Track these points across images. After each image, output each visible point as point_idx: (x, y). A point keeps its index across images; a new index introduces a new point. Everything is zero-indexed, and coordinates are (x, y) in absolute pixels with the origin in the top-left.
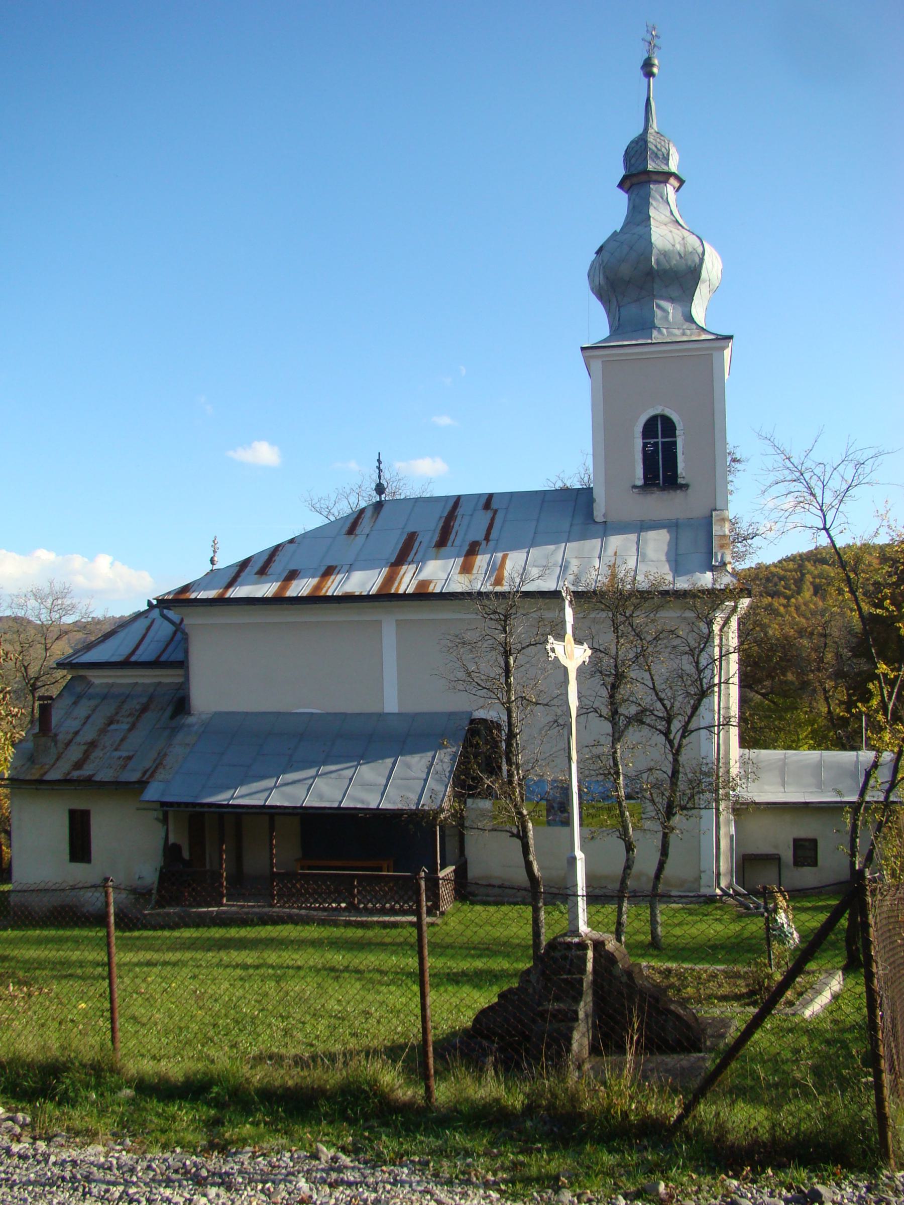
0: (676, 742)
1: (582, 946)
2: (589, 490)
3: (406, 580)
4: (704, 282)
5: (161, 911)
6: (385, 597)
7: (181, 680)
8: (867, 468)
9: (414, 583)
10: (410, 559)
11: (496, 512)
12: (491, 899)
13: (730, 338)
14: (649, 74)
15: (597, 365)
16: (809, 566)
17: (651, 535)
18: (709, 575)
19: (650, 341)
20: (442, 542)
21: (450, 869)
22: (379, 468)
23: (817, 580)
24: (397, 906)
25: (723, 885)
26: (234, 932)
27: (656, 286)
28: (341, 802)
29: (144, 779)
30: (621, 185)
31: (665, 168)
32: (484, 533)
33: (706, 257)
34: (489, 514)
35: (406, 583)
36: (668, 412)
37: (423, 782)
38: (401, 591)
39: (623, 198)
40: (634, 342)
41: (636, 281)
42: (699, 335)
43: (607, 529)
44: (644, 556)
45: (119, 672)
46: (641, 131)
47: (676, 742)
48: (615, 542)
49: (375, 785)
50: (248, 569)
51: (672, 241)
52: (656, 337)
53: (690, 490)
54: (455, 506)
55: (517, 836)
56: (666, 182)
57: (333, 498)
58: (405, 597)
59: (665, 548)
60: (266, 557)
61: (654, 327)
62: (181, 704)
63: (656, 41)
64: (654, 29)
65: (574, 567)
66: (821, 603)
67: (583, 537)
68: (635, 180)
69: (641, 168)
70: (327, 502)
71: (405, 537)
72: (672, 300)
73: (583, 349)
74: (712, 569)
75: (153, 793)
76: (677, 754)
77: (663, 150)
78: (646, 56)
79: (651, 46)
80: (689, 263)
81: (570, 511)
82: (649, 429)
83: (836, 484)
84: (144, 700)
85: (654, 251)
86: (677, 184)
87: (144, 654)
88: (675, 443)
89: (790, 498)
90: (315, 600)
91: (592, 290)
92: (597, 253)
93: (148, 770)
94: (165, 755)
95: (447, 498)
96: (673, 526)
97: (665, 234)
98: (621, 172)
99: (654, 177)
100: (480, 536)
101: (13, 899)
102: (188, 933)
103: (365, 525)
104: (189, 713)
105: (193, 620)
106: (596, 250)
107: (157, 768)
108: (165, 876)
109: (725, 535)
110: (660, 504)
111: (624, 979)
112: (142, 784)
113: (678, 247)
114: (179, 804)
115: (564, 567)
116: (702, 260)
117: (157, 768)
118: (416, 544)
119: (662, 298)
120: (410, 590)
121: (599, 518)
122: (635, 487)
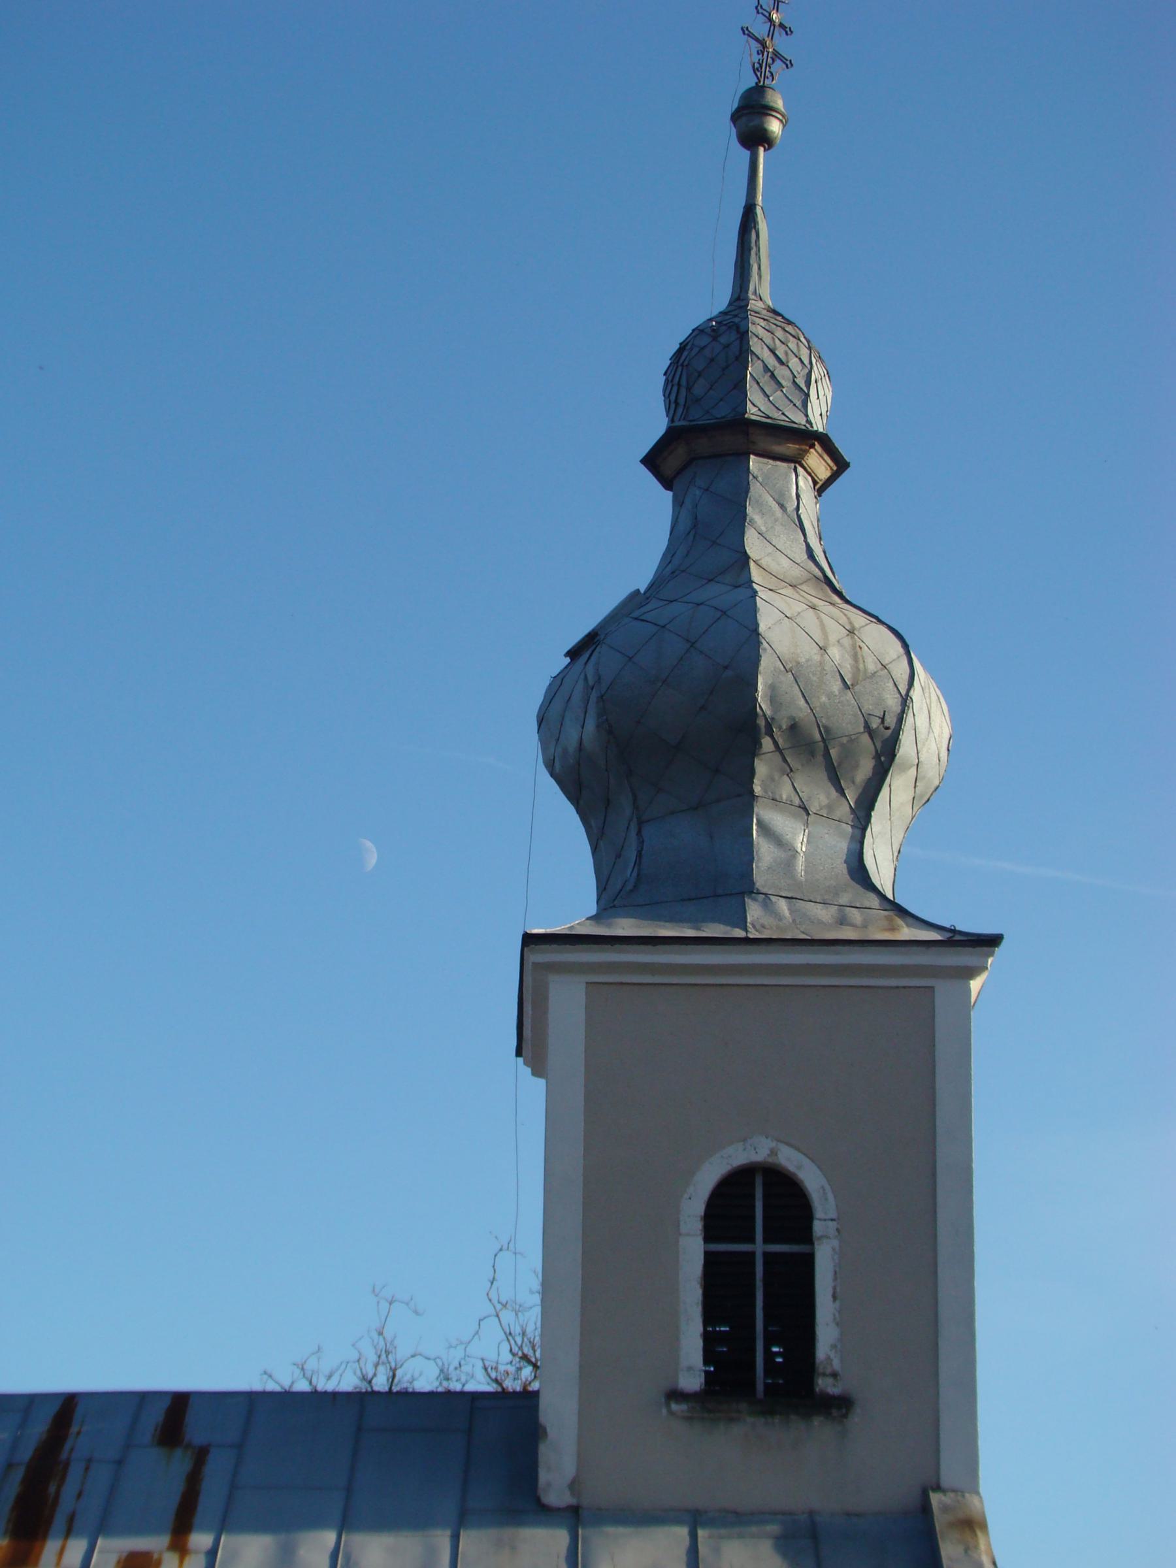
2: (528, 1399)
4: (904, 768)
11: (201, 1455)
13: (991, 941)
14: (754, 138)
15: (568, 1001)
19: (739, 933)
30: (652, 461)
31: (799, 419)
34: (180, 1463)
36: (790, 1159)
41: (667, 740)
46: (721, 301)
53: (856, 1418)
63: (780, 43)
69: (723, 412)
73: (529, 940)
78: (751, 81)
79: (767, 58)
82: (729, 1206)
85: (767, 663)
88: (807, 1263)
91: (550, 766)
92: (574, 654)
98: (656, 425)
121: (556, 1494)
122: (675, 1395)
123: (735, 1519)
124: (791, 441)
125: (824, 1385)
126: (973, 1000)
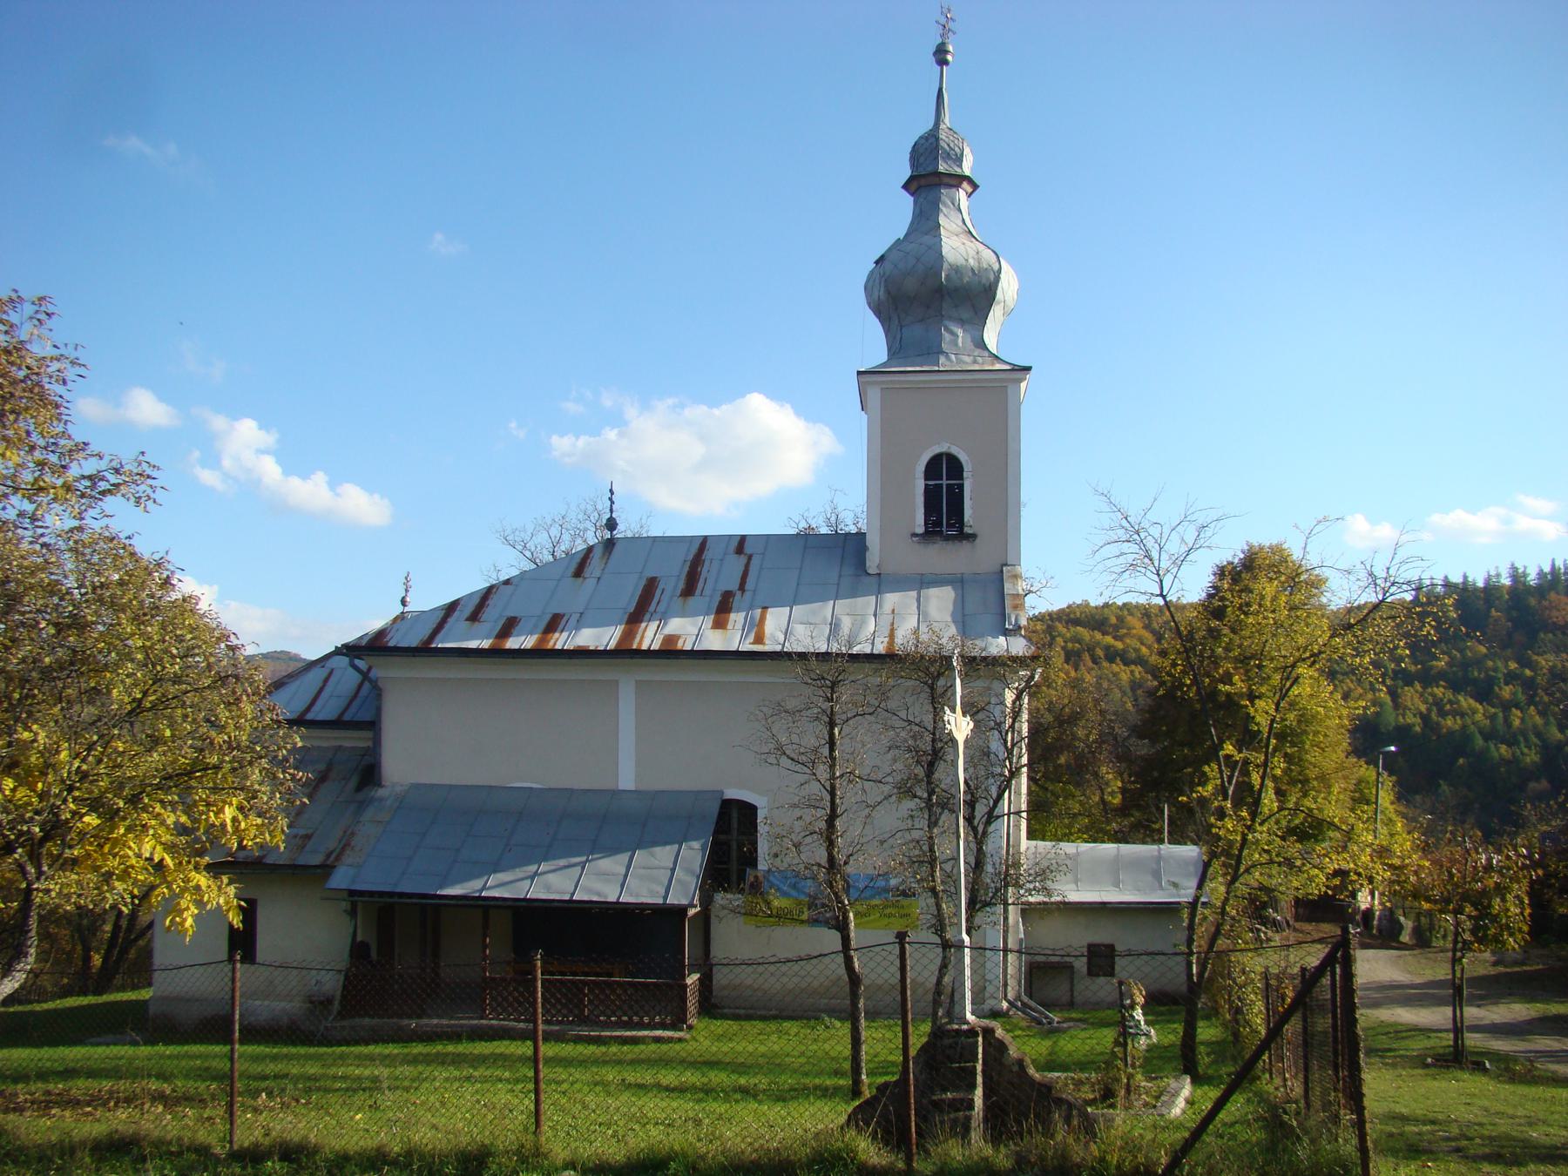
0: (980, 829)
1: (972, 1033)
2: (861, 536)
3: (650, 633)
5: (345, 1023)
6: (624, 653)
7: (370, 744)
8: (1208, 532)
9: (660, 638)
10: (652, 608)
11: (750, 557)
12: (742, 1012)
13: (1028, 369)
14: (942, 62)
15: (874, 395)
16: (1060, 627)
18: (1002, 638)
20: (689, 590)
21: (696, 976)
23: (1070, 645)
25: (1010, 996)
26: (463, 1048)
27: (945, 305)
30: (906, 187)
32: (738, 581)
34: (743, 559)
35: (649, 637)
36: (955, 451)
38: (644, 647)
41: (923, 300)
43: (882, 583)
44: (926, 614)
45: (343, 733)
46: (931, 125)
47: (980, 829)
48: (891, 599)
55: (837, 929)
56: (958, 186)
58: (649, 654)
59: (951, 607)
60: (476, 601)
62: (369, 774)
63: (951, 25)
65: (846, 624)
66: (1073, 674)
67: (854, 594)
68: (923, 182)
69: (930, 169)
72: (962, 322)
74: (1006, 633)
75: (341, 879)
78: (939, 41)
81: (836, 559)
83: (1174, 547)
84: (322, 767)
85: (945, 266)
86: (970, 190)
87: (321, 712)
88: (961, 487)
89: (1122, 560)
92: (877, 262)
94: (353, 834)
96: (958, 582)
97: (957, 246)
98: (906, 173)
99: (946, 180)
100: (733, 585)
101: (152, 1010)
104: (380, 785)
105: (385, 671)
107: (343, 849)
110: (943, 557)
111: (1016, 1068)
112: (326, 869)
113: (971, 262)
114: (371, 894)
115: (835, 627)
116: (997, 279)
117: (343, 849)
118: (658, 592)
119: (950, 318)
121: (872, 567)
122: (914, 535)
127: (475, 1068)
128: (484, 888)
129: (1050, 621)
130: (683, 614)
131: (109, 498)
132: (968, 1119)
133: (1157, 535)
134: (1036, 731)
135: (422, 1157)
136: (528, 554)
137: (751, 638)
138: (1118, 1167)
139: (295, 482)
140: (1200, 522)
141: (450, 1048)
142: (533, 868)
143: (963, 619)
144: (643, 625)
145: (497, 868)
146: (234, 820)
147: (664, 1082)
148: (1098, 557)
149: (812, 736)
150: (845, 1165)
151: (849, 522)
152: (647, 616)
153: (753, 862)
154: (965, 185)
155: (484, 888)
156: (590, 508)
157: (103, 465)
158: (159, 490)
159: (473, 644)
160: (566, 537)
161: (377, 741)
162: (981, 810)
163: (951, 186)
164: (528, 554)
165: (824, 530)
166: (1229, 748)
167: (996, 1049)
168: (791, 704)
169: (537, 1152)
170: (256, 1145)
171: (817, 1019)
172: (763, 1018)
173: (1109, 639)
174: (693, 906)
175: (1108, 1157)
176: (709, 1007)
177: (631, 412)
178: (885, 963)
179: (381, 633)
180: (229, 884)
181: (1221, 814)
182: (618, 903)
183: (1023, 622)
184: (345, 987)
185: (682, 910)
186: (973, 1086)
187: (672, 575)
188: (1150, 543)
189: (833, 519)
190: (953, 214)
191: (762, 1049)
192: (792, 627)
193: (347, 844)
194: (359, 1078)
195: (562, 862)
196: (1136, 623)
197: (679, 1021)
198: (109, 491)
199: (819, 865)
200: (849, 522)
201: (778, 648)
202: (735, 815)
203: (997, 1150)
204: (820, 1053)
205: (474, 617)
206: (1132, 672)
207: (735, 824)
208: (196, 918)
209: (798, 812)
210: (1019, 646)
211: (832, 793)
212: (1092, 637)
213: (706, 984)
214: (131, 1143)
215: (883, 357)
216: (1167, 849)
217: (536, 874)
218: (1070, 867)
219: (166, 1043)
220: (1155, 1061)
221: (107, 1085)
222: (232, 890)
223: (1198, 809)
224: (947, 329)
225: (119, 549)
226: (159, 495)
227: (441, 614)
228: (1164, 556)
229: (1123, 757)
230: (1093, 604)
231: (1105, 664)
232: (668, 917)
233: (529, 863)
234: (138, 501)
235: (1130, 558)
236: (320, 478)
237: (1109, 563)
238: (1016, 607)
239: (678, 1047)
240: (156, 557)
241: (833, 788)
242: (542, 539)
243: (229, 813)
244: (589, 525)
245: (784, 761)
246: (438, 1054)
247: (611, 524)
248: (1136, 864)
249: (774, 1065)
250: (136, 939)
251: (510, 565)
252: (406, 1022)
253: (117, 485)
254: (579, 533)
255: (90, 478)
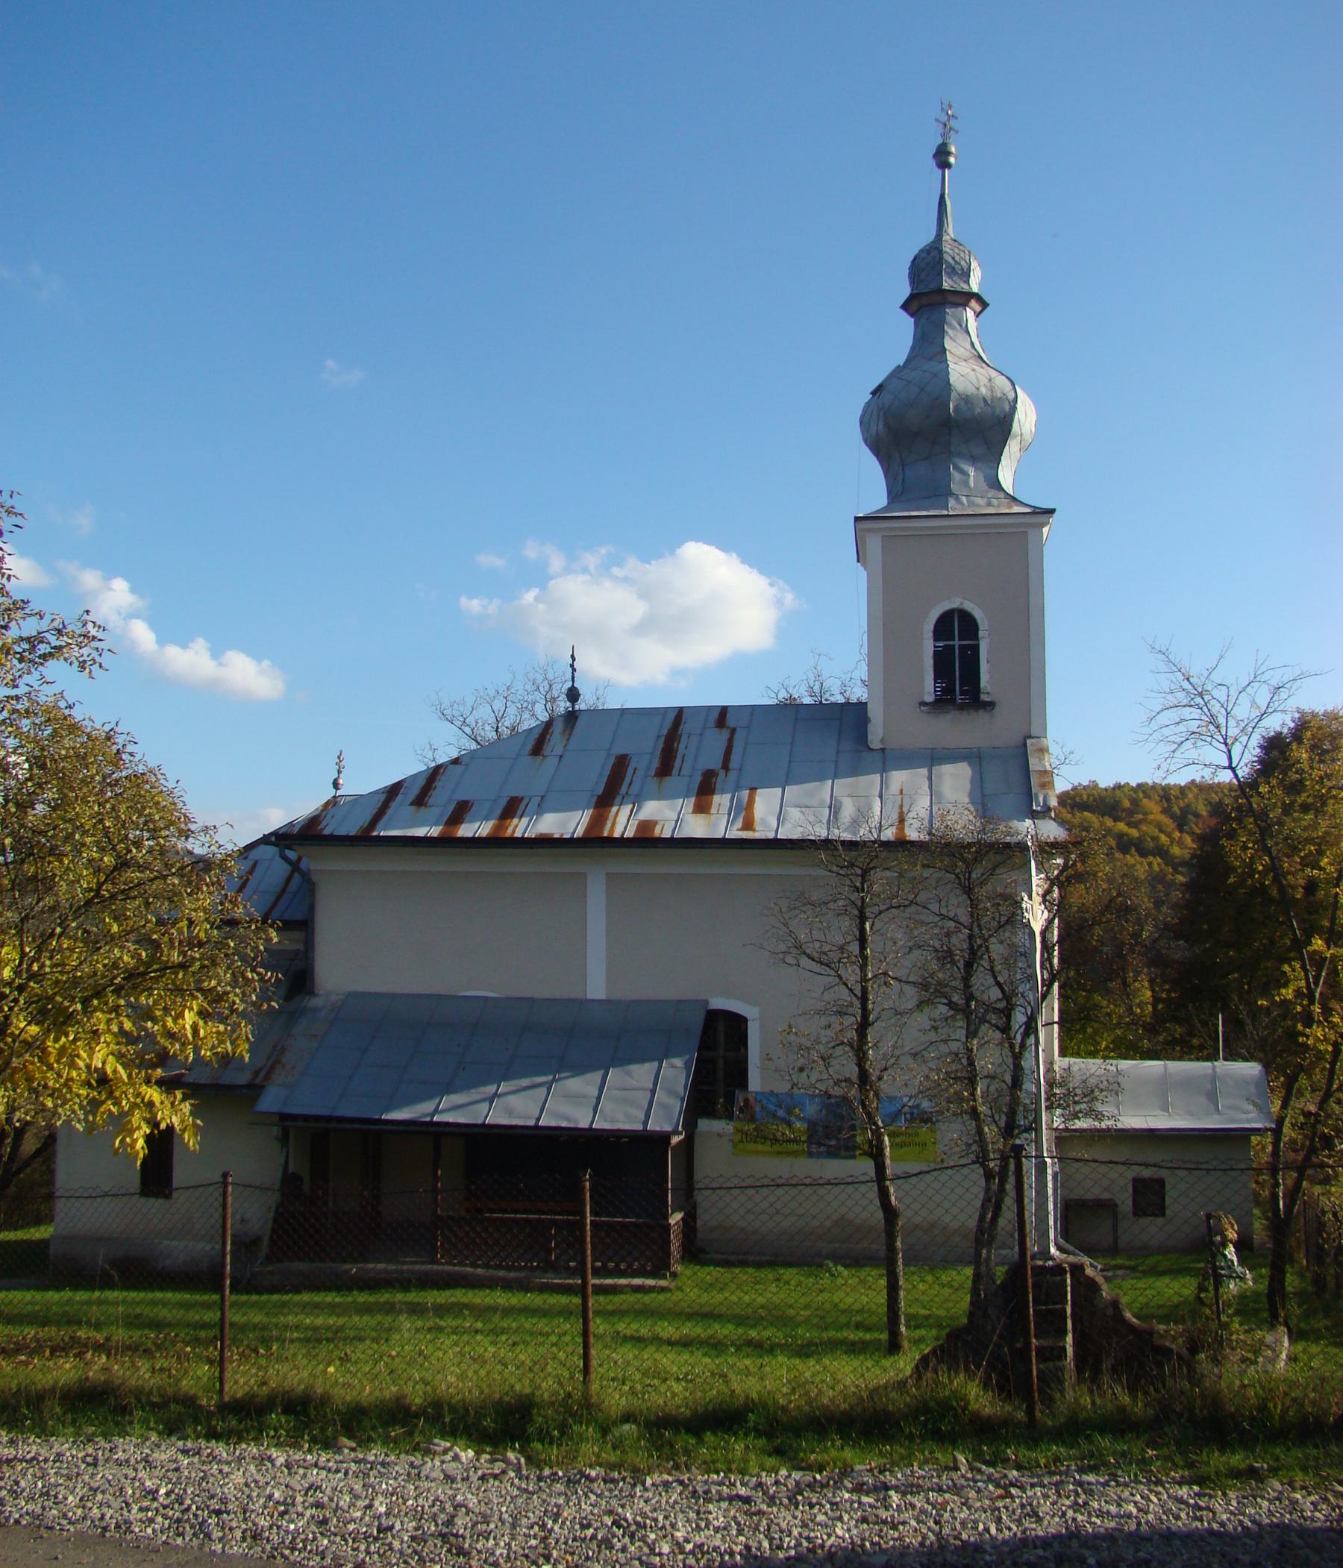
1: (1059, 1269)
2: (861, 706)
4: (1015, 437)
6: (594, 842)
7: (301, 947)
8: (1283, 694)
10: (623, 789)
11: (733, 731)
14: (943, 165)
15: (874, 545)
17: (947, 769)
18: (1028, 822)
19: (945, 512)
20: (665, 767)
22: (572, 666)
24: (623, 1266)
28: (538, 1119)
29: (258, 1081)
30: (905, 307)
31: (965, 287)
33: (1019, 405)
34: (725, 734)
35: (622, 822)
36: (969, 606)
37: (649, 1094)
38: (617, 834)
39: (909, 322)
40: (925, 513)
41: (927, 434)
42: (1010, 507)
43: (887, 760)
44: (940, 795)
46: (932, 237)
48: (899, 778)
49: (584, 1097)
50: (399, 798)
51: (975, 382)
52: (953, 507)
53: (997, 709)
54: (675, 724)
55: (871, 1155)
56: (965, 305)
57: (470, 702)
58: (622, 842)
59: (968, 786)
60: (422, 782)
61: (950, 494)
63: (952, 123)
64: (950, 107)
65: (848, 810)
67: (855, 772)
68: (925, 300)
69: (933, 286)
70: (461, 708)
71: (612, 761)
72: (974, 460)
73: (857, 519)
74: (1034, 815)
75: (270, 1101)
76: (1017, 1057)
77: (963, 263)
78: (940, 141)
79: (946, 129)
80: (998, 412)
81: (830, 734)
82: (944, 626)
85: (953, 395)
86: (978, 308)
88: (976, 649)
89: (1181, 727)
90: (496, 842)
91: (865, 441)
92: (874, 393)
93: (261, 1069)
94: (283, 1049)
95: (666, 710)
96: (975, 757)
97: (966, 374)
98: (906, 291)
99: (951, 298)
100: (715, 763)
101: (52, 1250)
102: (330, 1297)
103: (556, 743)
104: (312, 992)
105: (316, 862)
106: (872, 389)
108: (281, 1219)
109: (1045, 771)
110: (957, 729)
112: (254, 1090)
113: (983, 390)
114: (306, 1118)
115: (835, 809)
116: (1013, 409)
118: (630, 772)
119: (960, 455)
120: (630, 833)
121: (875, 742)
122: (923, 704)
123: (951, 756)
124: (965, 298)
125: (984, 697)
126: (1056, 921)
127: (441, 1318)
128: (436, 1111)
129: (1077, 801)
130: (659, 797)
131: (51, 663)
132: (1062, 1369)
133: (1223, 699)
134: (1074, 931)
135: (453, 1409)
136: (468, 730)
137: (739, 824)
138: (1282, 1417)
139: (173, 651)
140: (1274, 683)
141: (399, 1296)
142: (491, 1089)
143: (982, 801)
144: (614, 809)
145: (449, 1089)
146: (195, 1029)
147: (665, 1335)
148: (1154, 725)
149: (840, 931)
150: (955, 1415)
151: (836, 690)
152: (618, 799)
153: (743, 1083)
154: (973, 303)
155: (436, 1111)
156: (540, 678)
157: (44, 625)
158: (106, 653)
159: (420, 832)
160: (512, 710)
161: (309, 944)
162: (1019, 1018)
163: (957, 305)
164: (468, 730)
165: (807, 700)
166: (1318, 943)
167: (1086, 1288)
168: (816, 896)
169: (587, 1404)
170: (251, 1396)
171: (821, 1265)
172: (759, 1265)
173: (1121, 826)
174: (676, 1132)
175: (1271, 1405)
176: (694, 1253)
177: (557, 563)
178: (865, 1202)
179: (314, 821)
180: (183, 1100)
181: (1308, 1020)
182: (590, 1129)
183: (1053, 802)
184: (274, 1230)
185: (664, 1138)
186: (1065, 1333)
187: (645, 753)
188: (1215, 707)
189: (817, 688)
190: (961, 337)
191: (761, 1300)
192: (781, 812)
193: (278, 1061)
194: (316, 1329)
195: (525, 1082)
196: (1153, 807)
197: (660, 1268)
198: (51, 654)
199: (847, 1080)
200: (836, 690)
201: (771, 835)
202: (721, 1027)
203: (1134, 1398)
204: (827, 1306)
205: (420, 801)
206: (1150, 864)
207: (721, 1038)
208: (149, 1139)
209: (824, 1021)
210: (1051, 830)
211: (864, 999)
212: (1102, 824)
213: (689, 1222)
214: (103, 1392)
215: (883, 501)
216: (1223, 1066)
217: (495, 1095)
218: (1114, 1087)
219: (75, 1288)
220: (1245, 1307)
221: (30, 1332)
222: (186, 1107)
223: (1248, 1021)
224: (956, 468)
225: (60, 722)
226: (106, 659)
227: (383, 797)
228: (1232, 723)
229: (1157, 961)
230: (1102, 785)
231: (1118, 855)
232: (645, 1147)
233: (485, 1083)
234: (82, 666)
235: (1193, 726)
236: (200, 644)
237: (1166, 731)
238: (1043, 786)
239: (662, 1297)
240: (107, 728)
241: (864, 991)
242: (484, 713)
243: (189, 1018)
244: (538, 696)
245: (805, 961)
246: (387, 1303)
247: (573, 695)
248: (1187, 1084)
249: (780, 1318)
250: (19, 1171)
251: (448, 745)
252: (348, 1266)
253: (60, 648)
254: (527, 707)
255: (28, 640)
